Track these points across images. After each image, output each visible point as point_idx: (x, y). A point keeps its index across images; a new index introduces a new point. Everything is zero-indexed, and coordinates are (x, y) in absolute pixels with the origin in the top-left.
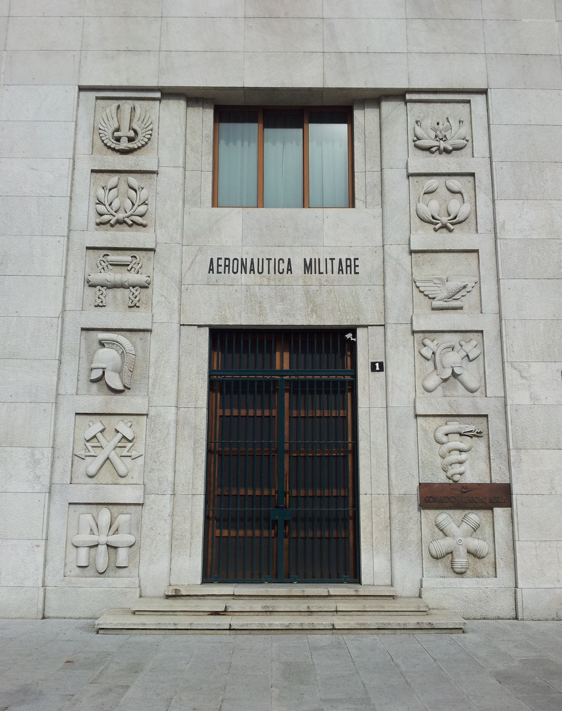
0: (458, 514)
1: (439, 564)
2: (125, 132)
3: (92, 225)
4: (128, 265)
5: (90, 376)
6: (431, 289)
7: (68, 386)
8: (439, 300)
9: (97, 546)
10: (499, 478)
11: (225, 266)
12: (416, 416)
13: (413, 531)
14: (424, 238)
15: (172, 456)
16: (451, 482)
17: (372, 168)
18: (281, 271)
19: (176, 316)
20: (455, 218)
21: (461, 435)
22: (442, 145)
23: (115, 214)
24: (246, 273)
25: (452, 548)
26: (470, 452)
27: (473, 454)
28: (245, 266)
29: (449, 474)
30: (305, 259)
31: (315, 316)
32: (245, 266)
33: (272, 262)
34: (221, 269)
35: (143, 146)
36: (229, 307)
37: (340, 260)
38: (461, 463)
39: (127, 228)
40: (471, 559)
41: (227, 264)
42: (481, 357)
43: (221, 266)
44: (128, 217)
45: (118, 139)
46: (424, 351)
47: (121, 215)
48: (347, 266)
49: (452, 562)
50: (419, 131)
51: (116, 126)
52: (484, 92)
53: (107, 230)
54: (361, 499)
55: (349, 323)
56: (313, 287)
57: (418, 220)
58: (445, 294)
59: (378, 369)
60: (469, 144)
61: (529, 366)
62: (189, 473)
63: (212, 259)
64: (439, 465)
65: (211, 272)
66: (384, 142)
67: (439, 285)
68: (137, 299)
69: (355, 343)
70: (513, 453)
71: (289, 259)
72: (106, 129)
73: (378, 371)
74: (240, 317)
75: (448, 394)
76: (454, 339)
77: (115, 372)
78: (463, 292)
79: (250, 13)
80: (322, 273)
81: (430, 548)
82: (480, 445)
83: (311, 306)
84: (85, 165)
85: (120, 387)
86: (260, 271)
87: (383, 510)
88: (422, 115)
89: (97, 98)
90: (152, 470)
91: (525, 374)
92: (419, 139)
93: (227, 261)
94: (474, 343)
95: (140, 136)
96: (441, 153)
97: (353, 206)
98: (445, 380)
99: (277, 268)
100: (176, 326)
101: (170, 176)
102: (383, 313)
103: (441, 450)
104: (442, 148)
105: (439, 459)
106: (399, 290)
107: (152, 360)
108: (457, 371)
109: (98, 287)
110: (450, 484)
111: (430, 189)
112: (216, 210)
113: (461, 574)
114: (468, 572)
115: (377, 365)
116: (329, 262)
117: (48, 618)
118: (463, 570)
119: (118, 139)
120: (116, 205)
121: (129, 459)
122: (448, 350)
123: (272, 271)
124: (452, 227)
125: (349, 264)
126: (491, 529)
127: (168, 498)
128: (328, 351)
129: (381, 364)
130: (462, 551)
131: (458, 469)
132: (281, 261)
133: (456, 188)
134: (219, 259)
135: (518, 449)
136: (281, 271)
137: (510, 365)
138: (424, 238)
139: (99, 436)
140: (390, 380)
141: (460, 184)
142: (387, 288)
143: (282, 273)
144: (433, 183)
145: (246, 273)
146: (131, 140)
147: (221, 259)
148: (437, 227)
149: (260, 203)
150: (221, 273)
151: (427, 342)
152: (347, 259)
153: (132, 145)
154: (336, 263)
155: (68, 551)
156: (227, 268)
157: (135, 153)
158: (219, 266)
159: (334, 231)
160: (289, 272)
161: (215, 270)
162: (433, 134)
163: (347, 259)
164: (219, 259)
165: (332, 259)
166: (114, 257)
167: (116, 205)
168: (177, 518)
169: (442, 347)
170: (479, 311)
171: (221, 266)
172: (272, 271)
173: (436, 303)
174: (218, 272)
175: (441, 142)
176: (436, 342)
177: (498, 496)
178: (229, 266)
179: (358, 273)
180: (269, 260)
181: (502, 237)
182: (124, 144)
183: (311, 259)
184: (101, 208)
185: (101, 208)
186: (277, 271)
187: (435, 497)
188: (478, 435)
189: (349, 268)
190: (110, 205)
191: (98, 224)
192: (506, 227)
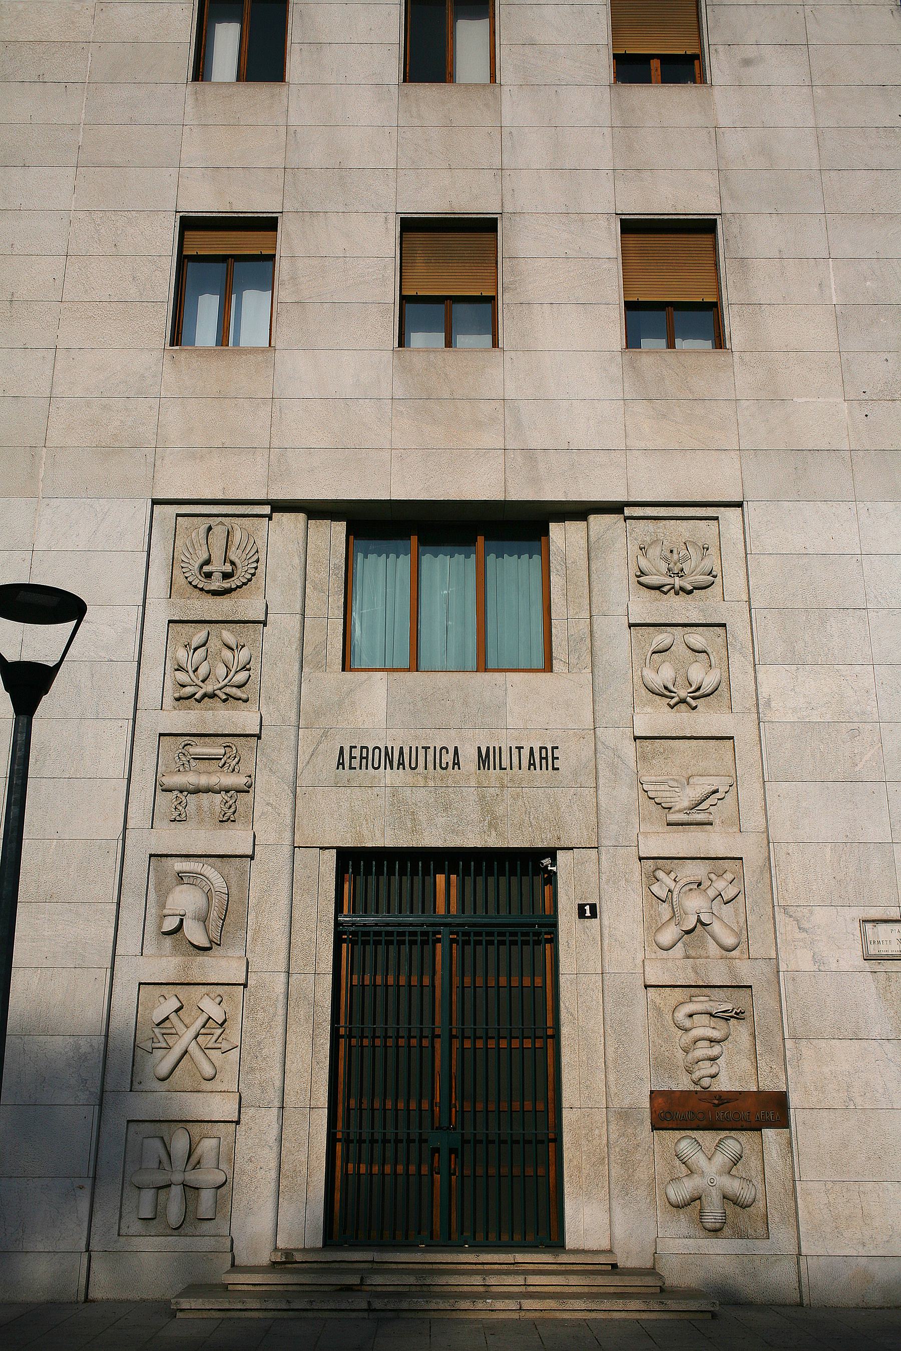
0: (708, 1138)
1: (682, 1216)
2: (217, 566)
3: (169, 701)
4: (221, 759)
5: (161, 927)
6: (668, 794)
7: (129, 943)
8: (680, 811)
9: (169, 1186)
10: (769, 1084)
11: (362, 758)
12: (646, 987)
13: (641, 1164)
14: (655, 718)
15: (279, 1048)
16: (698, 1088)
17: (577, 613)
18: (444, 766)
19: (288, 835)
20: (699, 688)
21: (711, 1015)
22: (678, 582)
23: (201, 684)
24: (392, 769)
25: (700, 1192)
26: (726, 1042)
27: (730, 1046)
28: (393, 759)
29: (696, 1076)
30: (479, 748)
31: (494, 833)
32: (393, 759)
33: (431, 752)
34: (356, 763)
35: (245, 584)
36: (367, 820)
37: (532, 748)
38: (713, 1059)
39: (220, 704)
40: (730, 1209)
41: (364, 755)
42: (741, 896)
43: (355, 758)
44: (220, 689)
45: (208, 575)
46: (655, 888)
47: (209, 688)
48: (541, 758)
49: (701, 1212)
50: (644, 563)
51: (205, 556)
52: (739, 505)
53: (190, 709)
54: (564, 1116)
55: (545, 845)
56: (492, 790)
57: (644, 691)
58: (686, 804)
59: (588, 914)
60: (718, 580)
61: (811, 913)
62: (306, 1074)
63: (342, 748)
64: (681, 1063)
65: (341, 766)
66: (594, 576)
67: (677, 789)
68: (232, 810)
69: (555, 873)
70: (789, 1044)
71: (456, 748)
72: (191, 561)
73: (588, 917)
74: (383, 835)
75: (693, 954)
76: (698, 870)
77: (199, 920)
78: (713, 800)
79: (399, 394)
80: (505, 769)
81: (668, 1192)
82: (740, 1032)
83: (488, 818)
84: (159, 613)
85: (205, 943)
86: (413, 766)
87: (597, 1132)
88: (648, 539)
89: (178, 515)
90: (252, 1070)
91: (806, 925)
92: (643, 573)
93: (365, 750)
94: (729, 876)
95: (239, 572)
96: (677, 593)
97: (705, 227)
98: (688, 932)
99: (438, 761)
100: (287, 850)
101: (283, 625)
102: (595, 830)
103: (682, 1040)
104: (677, 587)
105: (680, 1054)
106: (619, 796)
107: (253, 901)
108: (705, 919)
109: (176, 792)
110: (696, 1092)
111: (660, 648)
112: (348, 675)
113: (715, 1232)
114: (726, 1229)
115: (587, 908)
116: (515, 752)
117: (93, 1301)
118: (718, 1225)
119: (208, 575)
120: (203, 671)
121: (218, 1052)
122: (691, 886)
123: (430, 765)
124: (693, 703)
125: (544, 755)
126: (759, 1163)
127: (275, 1111)
128: (512, 888)
129: (593, 907)
130: (715, 1197)
131: (706, 1069)
132: (444, 751)
133: (698, 646)
134: (351, 748)
135: (794, 1038)
136: (444, 766)
137: (782, 910)
138: (655, 718)
139: (173, 1017)
140: (606, 932)
141: (704, 640)
142: (600, 792)
143: (446, 768)
144: (662, 638)
145: (392, 769)
146: (226, 576)
147: (355, 747)
148: (673, 702)
149: (415, 666)
150: (355, 768)
151: (660, 874)
152: (541, 748)
153: (226, 585)
154: (525, 753)
155: (125, 1195)
156: (364, 761)
157: (233, 594)
158: (351, 758)
159: (522, 707)
160: (456, 766)
161: (347, 765)
162: (663, 567)
163: (541, 748)
164: (351, 748)
165: (519, 748)
166: (201, 749)
167: (203, 671)
168: (287, 1144)
169: (682, 883)
170: (736, 829)
171: (355, 758)
172: (430, 765)
173: (673, 817)
174: (351, 768)
175: (677, 579)
176: (673, 875)
177: (771, 1110)
178: (367, 758)
179: (558, 769)
180: (426, 748)
181: (766, 719)
182: (216, 584)
183: (488, 748)
184: (182, 677)
185: (182, 677)
186: (438, 765)
187: (677, 1112)
188: (739, 1016)
189: (544, 761)
190: (194, 672)
191: (178, 699)
192: (773, 704)
